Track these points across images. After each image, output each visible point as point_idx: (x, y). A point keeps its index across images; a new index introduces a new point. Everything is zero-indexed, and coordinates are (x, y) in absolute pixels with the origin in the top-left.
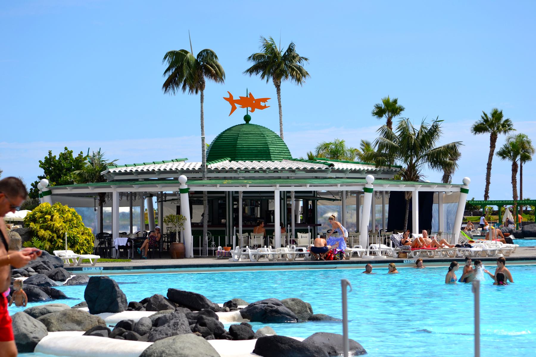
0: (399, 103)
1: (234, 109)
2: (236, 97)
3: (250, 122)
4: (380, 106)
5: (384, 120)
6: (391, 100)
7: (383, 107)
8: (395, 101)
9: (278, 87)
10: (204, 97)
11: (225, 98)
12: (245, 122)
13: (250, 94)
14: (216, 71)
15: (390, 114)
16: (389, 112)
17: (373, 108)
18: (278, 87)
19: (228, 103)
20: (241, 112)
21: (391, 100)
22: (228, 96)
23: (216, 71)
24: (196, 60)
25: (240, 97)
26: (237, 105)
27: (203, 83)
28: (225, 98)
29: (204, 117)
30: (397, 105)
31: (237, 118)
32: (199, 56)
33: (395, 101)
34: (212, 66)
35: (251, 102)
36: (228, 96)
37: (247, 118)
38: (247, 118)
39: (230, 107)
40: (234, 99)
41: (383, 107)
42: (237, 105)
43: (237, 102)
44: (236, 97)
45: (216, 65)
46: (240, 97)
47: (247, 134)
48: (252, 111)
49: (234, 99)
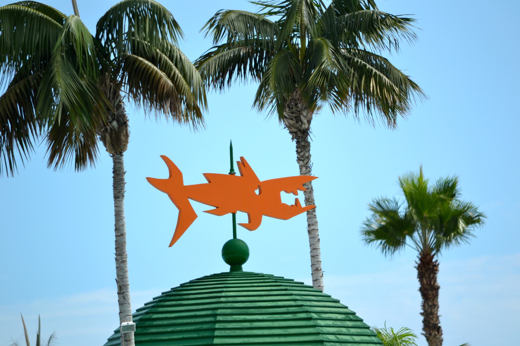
0: (465, 196)
1: (186, 218)
2: (193, 177)
3: (246, 267)
4: (392, 206)
5: (409, 252)
6: (432, 184)
7: (403, 208)
8: (449, 189)
9: (301, 136)
10: (126, 177)
11: (150, 180)
12: (226, 268)
13: (243, 163)
14: (173, 79)
15: (431, 237)
16: (424, 228)
17: (365, 216)
18: (301, 136)
19: (165, 196)
20: (212, 230)
21: (432, 184)
22: (164, 174)
23: (173, 79)
24: (97, 40)
25: (206, 175)
26: (197, 206)
27: (123, 123)
28: (150, 180)
29: (129, 249)
30: (454, 204)
31: (201, 256)
32: (101, 26)
33: (449, 189)
34: (154, 60)
35: (239, 191)
36: (164, 174)
37: (235, 253)
38: (235, 253)
39: (171, 213)
40: (187, 182)
41: (403, 208)
42: (197, 206)
43: (197, 192)
44: (193, 177)
45: (171, 58)
46: (206, 175)
47: (245, 310)
48: (253, 224)
49: (187, 182)
